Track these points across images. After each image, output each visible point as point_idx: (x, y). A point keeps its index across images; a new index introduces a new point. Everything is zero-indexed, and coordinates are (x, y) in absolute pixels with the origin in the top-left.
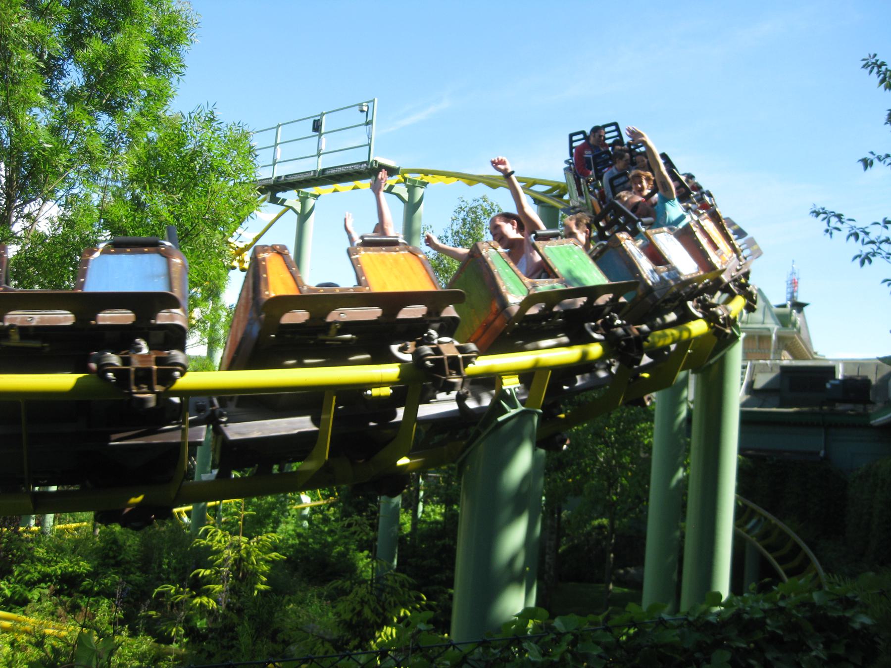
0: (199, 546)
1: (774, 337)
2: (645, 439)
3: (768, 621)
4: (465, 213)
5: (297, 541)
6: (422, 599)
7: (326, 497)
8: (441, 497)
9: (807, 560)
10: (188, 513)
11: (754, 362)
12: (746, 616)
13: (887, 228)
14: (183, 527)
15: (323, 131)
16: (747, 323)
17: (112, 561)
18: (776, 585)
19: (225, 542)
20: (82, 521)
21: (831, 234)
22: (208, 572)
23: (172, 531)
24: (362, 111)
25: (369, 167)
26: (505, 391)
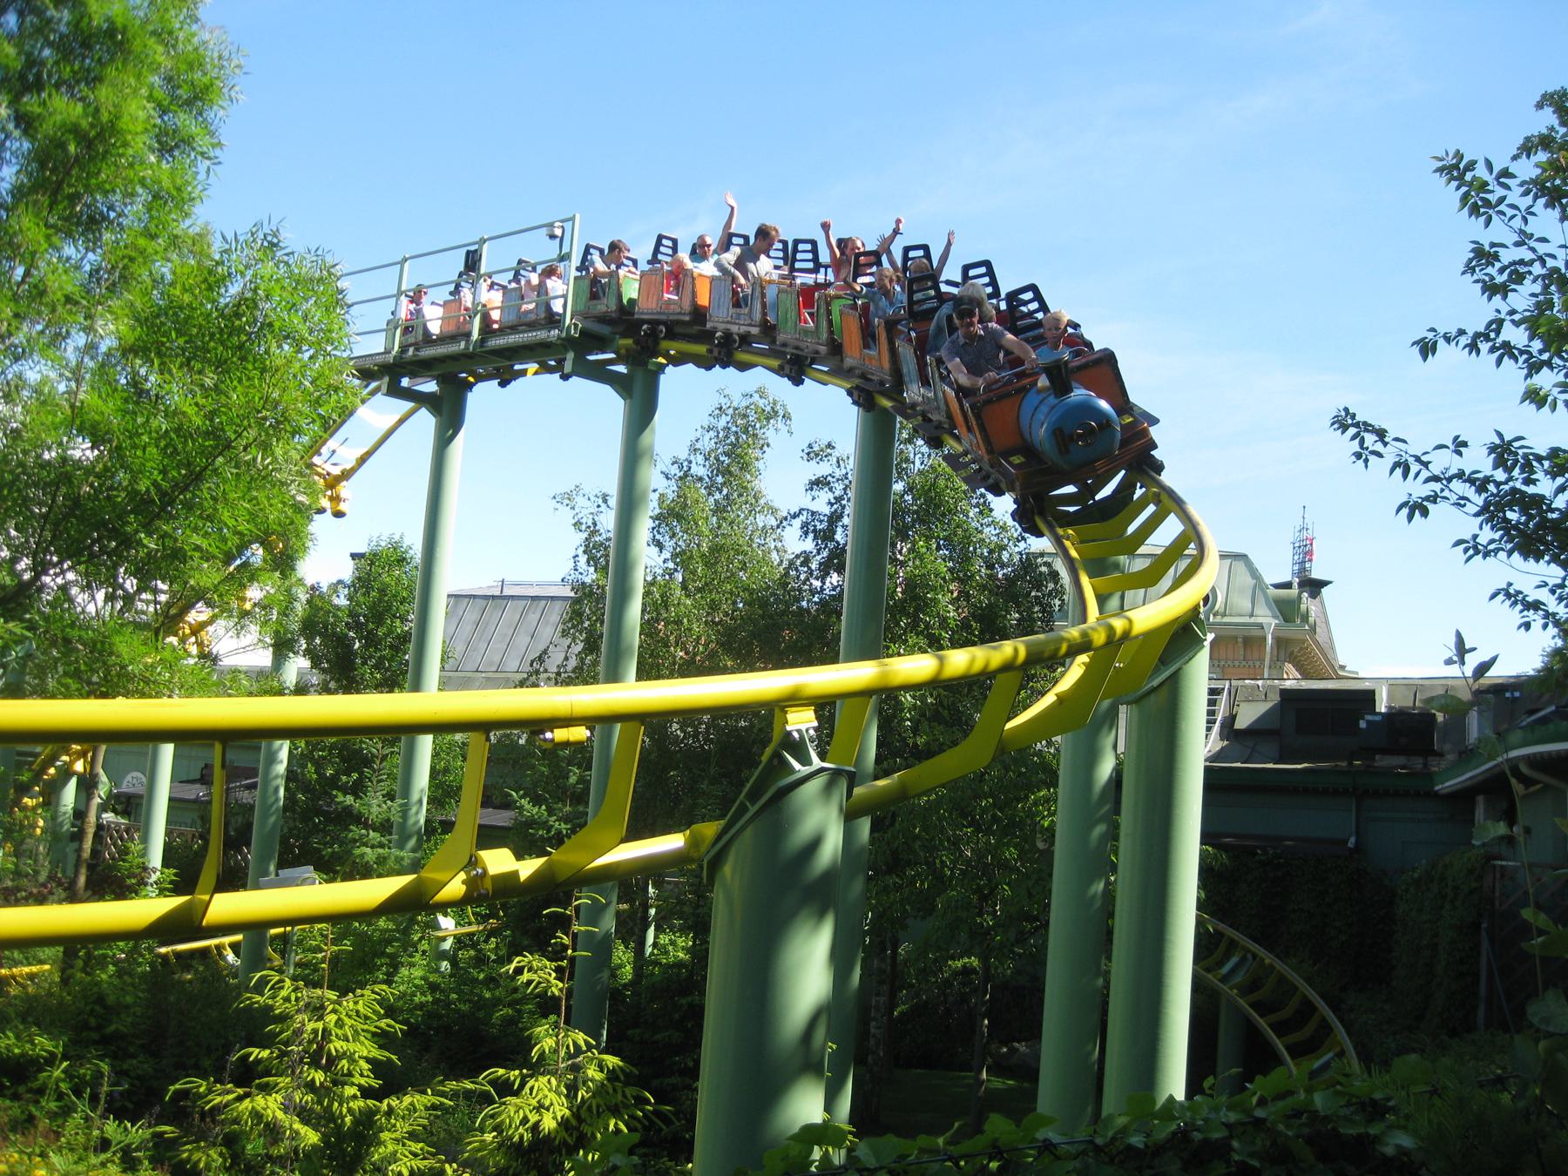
0: (249, 1008)
1: (1269, 638)
2: (1043, 818)
3: (1235, 1144)
4: (729, 418)
5: (430, 998)
6: (647, 1102)
7: (481, 919)
8: (686, 921)
9: (1325, 1027)
10: (235, 947)
11: (1234, 683)
12: (1197, 1136)
13: (1460, 454)
14: (225, 973)
15: (482, 271)
16: (1224, 615)
17: (95, 1036)
18: (1251, 1082)
19: (297, 999)
20: (42, 962)
21: (1366, 461)
22: (265, 1054)
23: (204, 980)
24: (552, 237)
25: (564, 335)
26: (789, 733)
